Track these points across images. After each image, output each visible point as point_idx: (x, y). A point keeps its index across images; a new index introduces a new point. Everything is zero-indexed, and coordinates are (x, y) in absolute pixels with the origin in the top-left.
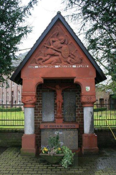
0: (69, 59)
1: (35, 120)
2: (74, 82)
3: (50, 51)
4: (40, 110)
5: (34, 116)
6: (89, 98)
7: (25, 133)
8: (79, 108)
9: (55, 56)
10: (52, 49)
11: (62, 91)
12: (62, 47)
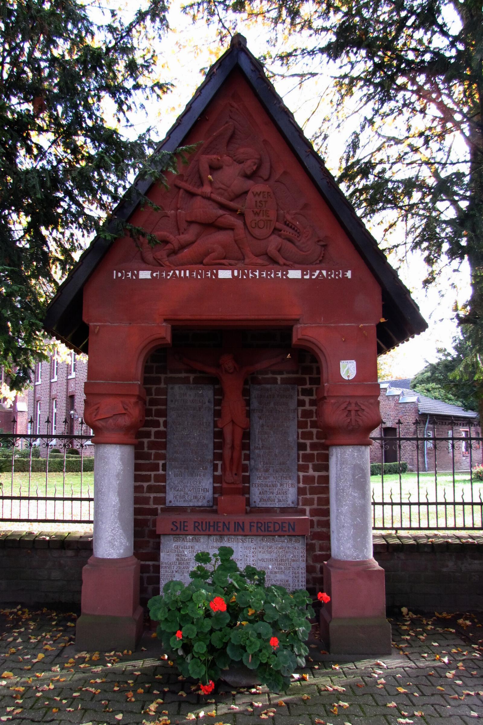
0: (274, 242)
1: (137, 501)
2: (294, 340)
3: (201, 209)
4: (159, 457)
5: (131, 483)
6: (353, 407)
7: (95, 553)
8: (308, 451)
9: (220, 228)
10: (209, 199)
11: (246, 382)
12: (246, 193)
